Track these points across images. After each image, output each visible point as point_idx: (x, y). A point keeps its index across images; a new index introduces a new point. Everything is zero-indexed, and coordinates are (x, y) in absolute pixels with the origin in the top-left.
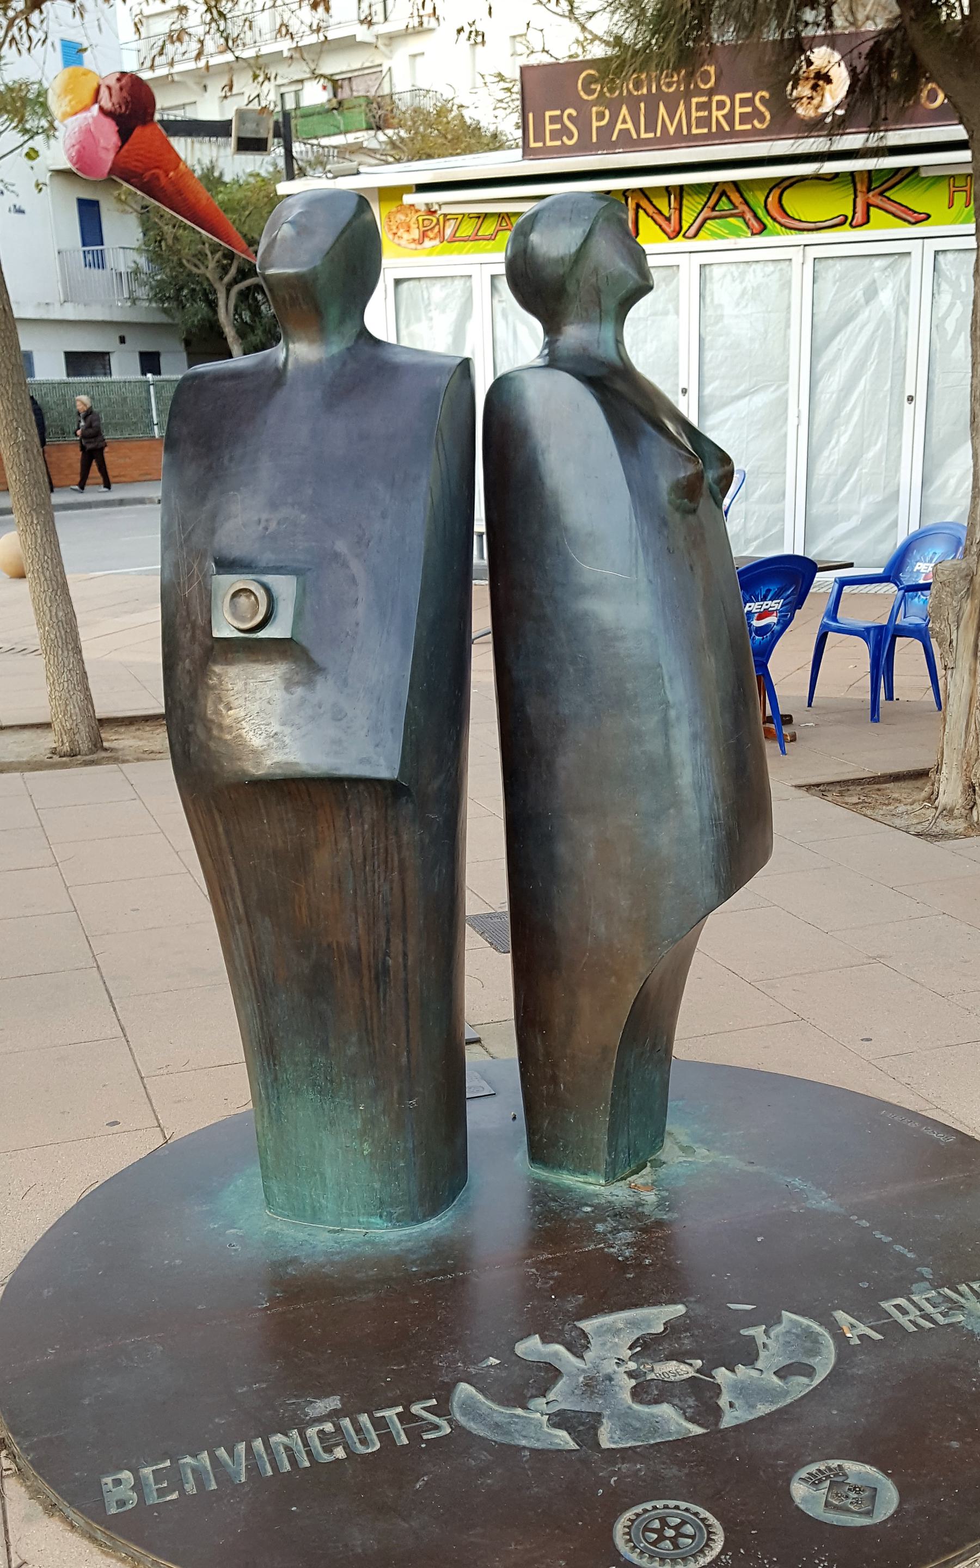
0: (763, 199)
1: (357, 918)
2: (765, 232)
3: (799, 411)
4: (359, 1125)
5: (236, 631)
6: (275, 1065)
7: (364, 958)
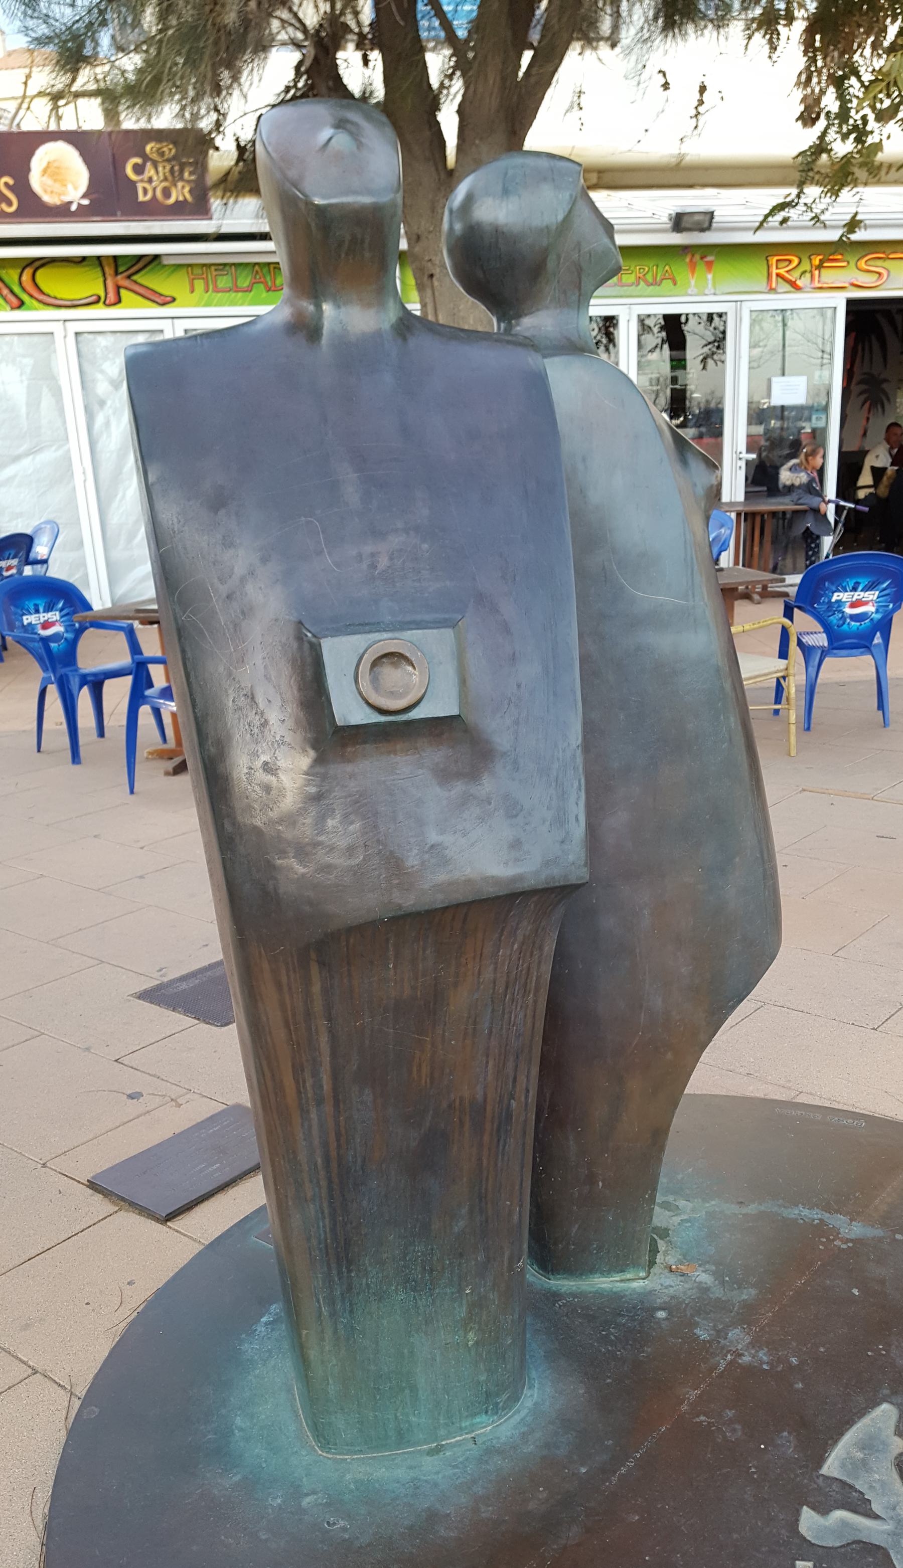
0: (16, 277)
1: (487, 1062)
2: (23, 307)
3: (84, 469)
4: (462, 1312)
5: (368, 710)
6: (349, 1271)
7: (489, 1108)
